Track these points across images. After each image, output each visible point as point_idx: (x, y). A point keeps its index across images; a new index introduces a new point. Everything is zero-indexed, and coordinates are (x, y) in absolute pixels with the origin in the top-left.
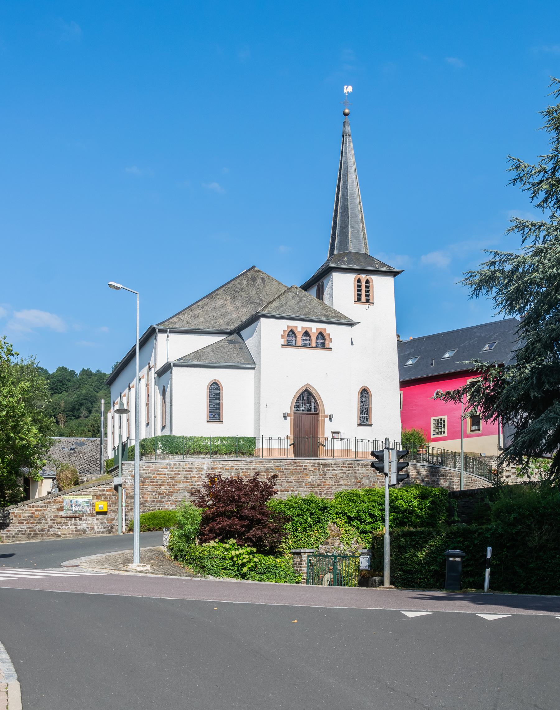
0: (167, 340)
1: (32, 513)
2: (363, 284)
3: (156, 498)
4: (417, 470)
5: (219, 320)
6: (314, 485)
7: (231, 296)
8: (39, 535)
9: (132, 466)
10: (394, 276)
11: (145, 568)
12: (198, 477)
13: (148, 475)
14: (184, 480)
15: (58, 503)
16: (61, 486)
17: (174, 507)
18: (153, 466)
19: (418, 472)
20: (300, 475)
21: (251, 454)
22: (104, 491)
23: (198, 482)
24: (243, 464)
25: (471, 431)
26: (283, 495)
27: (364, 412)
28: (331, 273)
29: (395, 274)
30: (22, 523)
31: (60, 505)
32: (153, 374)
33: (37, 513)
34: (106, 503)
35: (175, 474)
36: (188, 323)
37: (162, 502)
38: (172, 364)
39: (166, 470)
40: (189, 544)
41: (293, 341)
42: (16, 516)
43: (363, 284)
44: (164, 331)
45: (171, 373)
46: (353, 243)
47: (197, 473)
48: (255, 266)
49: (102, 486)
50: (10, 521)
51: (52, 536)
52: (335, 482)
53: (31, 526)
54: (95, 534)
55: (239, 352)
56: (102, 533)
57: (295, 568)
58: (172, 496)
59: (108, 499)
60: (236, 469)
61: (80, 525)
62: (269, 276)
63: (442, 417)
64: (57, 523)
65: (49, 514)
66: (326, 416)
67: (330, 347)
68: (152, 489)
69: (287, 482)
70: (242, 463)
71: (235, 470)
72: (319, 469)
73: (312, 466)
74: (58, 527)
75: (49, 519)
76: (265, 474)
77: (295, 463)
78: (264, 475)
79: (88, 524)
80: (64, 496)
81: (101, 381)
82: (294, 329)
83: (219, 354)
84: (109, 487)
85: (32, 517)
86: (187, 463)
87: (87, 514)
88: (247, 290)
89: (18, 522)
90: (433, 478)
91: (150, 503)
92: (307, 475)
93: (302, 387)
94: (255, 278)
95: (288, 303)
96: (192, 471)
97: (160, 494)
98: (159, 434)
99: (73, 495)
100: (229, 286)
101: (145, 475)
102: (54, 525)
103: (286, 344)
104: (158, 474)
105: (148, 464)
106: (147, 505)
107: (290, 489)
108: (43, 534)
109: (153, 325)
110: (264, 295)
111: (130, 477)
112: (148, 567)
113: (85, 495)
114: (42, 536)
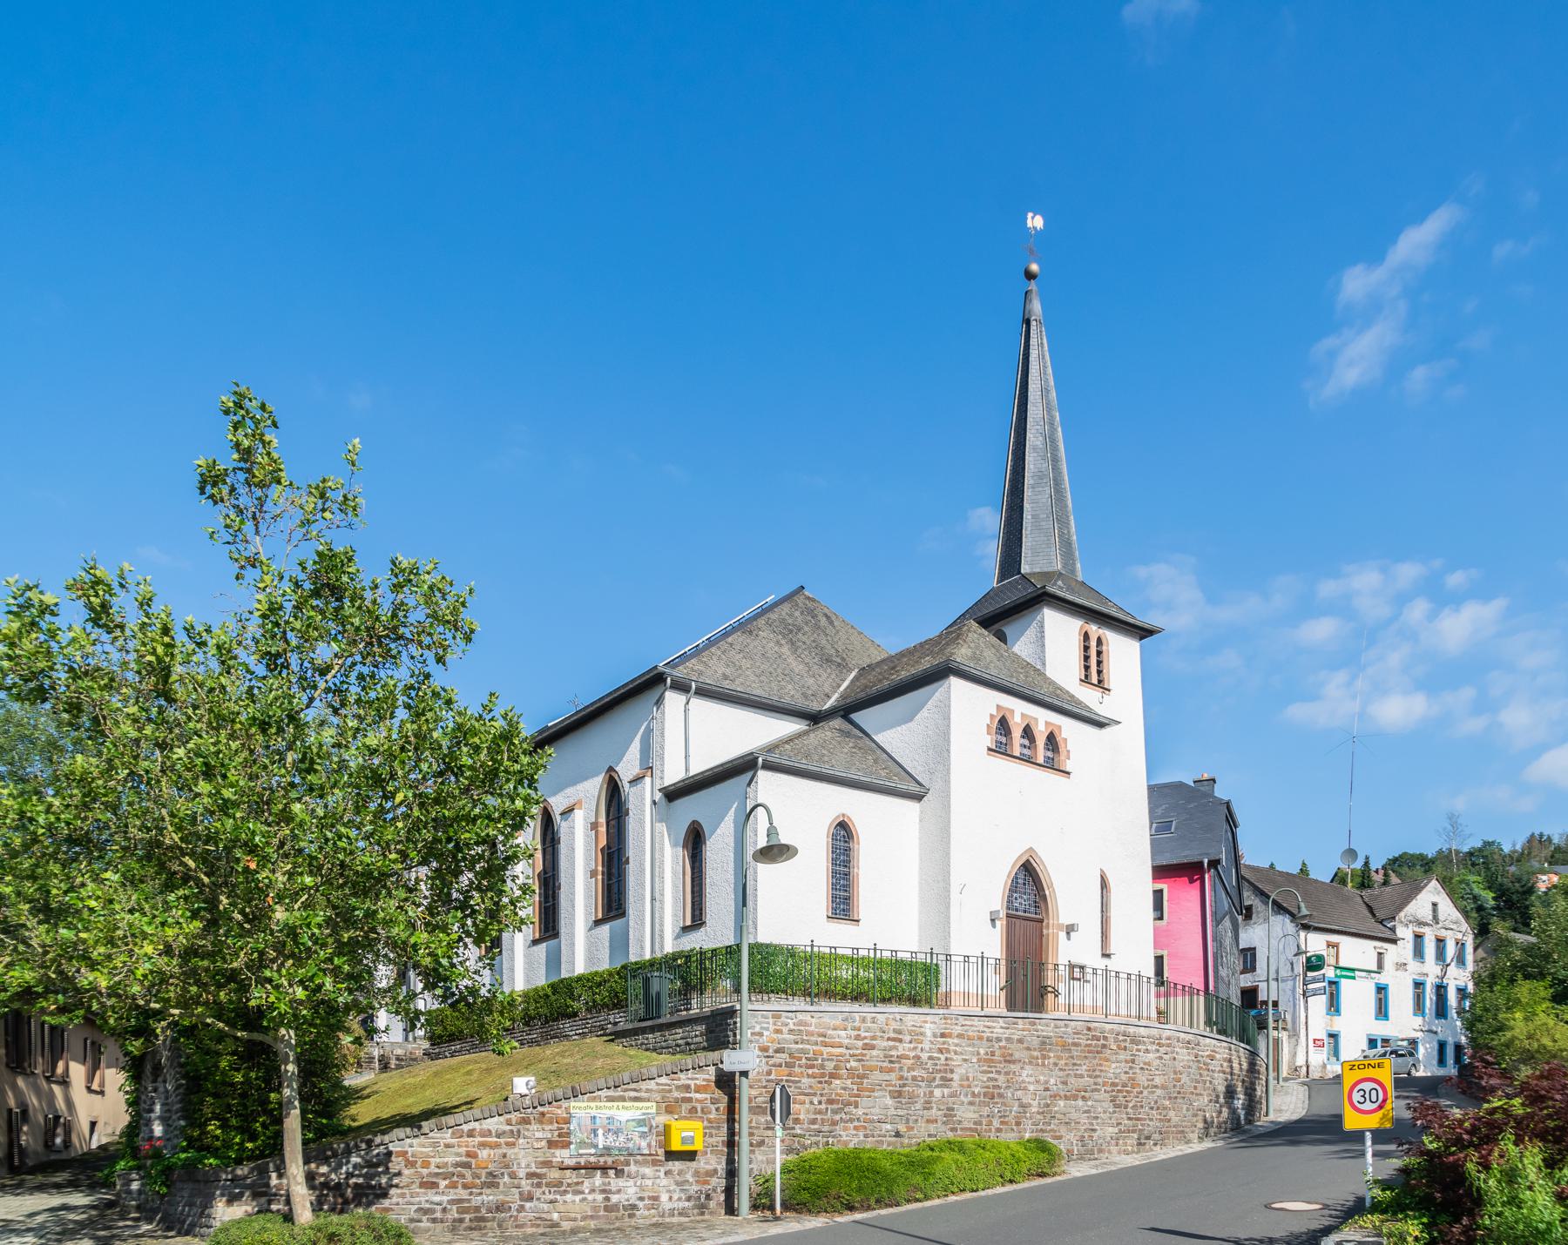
1: (468, 1155)
2: (1093, 644)
3: (820, 1112)
6: (1116, 1085)
8: (489, 1224)
9: (760, 1019)
12: (914, 1057)
13: (801, 1046)
15: (551, 1123)
17: (862, 1138)
18: (813, 1020)
22: (687, 1088)
24: (1002, 1028)
26: (1069, 1110)
28: (1041, 608)
29: (1142, 633)
30: (434, 1185)
31: (559, 1129)
33: (484, 1154)
34: (699, 1125)
36: (725, 677)
37: (834, 1123)
39: (843, 1033)
43: (1093, 644)
44: (681, 687)
47: (912, 1046)
49: (682, 1076)
50: (390, 1179)
51: (532, 1226)
52: (1148, 1080)
53: (462, 1193)
54: (663, 1216)
59: (699, 1114)
60: (989, 1040)
61: (619, 1191)
64: (548, 1185)
65: (524, 1158)
66: (1060, 927)
67: (1068, 770)
69: (1076, 1076)
71: (985, 1042)
72: (1125, 1048)
74: (551, 1197)
75: (522, 1173)
77: (1089, 1029)
79: (642, 1188)
80: (573, 1104)
85: (467, 1165)
86: (891, 1017)
87: (639, 1157)
89: (418, 1181)
96: (900, 1041)
97: (830, 1102)
101: (793, 1046)
102: (538, 1193)
103: (994, 748)
105: (800, 1016)
106: (799, 1132)
108: (504, 1220)
113: (636, 1099)
114: (500, 1226)
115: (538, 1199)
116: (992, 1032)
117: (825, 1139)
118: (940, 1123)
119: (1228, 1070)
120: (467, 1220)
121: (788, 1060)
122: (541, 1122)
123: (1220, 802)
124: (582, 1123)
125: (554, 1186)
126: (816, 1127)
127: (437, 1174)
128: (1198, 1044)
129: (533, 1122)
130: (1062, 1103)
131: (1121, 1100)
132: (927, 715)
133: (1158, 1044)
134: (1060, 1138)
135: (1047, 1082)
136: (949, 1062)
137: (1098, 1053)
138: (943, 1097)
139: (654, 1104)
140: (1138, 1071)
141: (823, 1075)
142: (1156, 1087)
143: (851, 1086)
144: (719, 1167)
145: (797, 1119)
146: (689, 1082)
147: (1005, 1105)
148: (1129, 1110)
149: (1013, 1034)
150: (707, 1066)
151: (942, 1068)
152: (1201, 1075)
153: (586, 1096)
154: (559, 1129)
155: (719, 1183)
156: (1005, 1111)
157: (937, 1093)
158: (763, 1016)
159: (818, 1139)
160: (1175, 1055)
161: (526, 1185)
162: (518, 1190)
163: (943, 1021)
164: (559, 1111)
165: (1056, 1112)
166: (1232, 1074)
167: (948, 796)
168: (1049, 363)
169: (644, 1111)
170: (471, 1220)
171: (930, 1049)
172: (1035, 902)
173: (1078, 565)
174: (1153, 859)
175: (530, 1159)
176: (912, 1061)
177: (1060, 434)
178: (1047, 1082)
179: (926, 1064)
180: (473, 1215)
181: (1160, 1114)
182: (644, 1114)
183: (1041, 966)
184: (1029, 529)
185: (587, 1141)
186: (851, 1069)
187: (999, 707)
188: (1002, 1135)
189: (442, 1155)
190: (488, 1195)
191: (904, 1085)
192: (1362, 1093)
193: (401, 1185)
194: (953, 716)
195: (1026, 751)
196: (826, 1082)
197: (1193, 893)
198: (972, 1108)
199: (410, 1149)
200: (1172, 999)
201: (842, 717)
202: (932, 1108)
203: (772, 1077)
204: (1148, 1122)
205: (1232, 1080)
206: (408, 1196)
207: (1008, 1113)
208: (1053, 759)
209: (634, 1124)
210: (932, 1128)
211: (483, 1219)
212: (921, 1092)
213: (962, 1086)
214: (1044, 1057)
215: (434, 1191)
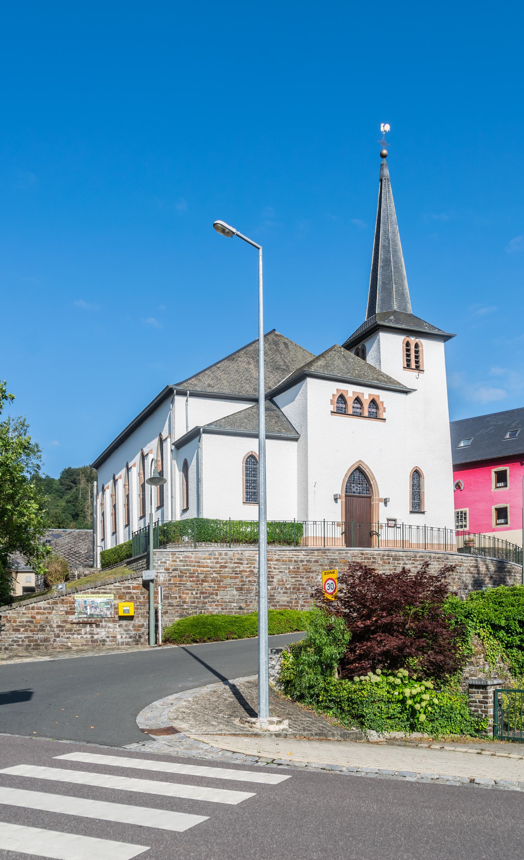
0: (187, 405)
1: (32, 617)
2: (412, 347)
3: (197, 598)
4: (486, 565)
5: (244, 385)
7: (253, 359)
8: (41, 647)
9: (165, 556)
11: (282, 727)
12: (249, 571)
13: (186, 568)
14: (233, 575)
15: (67, 604)
16: (49, 581)
17: (220, 610)
18: (193, 555)
19: (487, 568)
21: (297, 544)
22: (129, 588)
23: (249, 577)
24: (304, 555)
25: (497, 524)
27: (416, 497)
28: (379, 333)
29: (445, 338)
30: (18, 630)
31: (70, 606)
32: (168, 446)
33: (38, 617)
34: (132, 604)
35: (221, 567)
36: (209, 385)
37: (205, 603)
38: (201, 430)
39: (209, 561)
40: (326, 676)
41: (342, 408)
42: (9, 621)
43: (412, 347)
44: (183, 393)
45: (199, 441)
46: (397, 301)
47: (248, 566)
48: (275, 330)
49: (126, 582)
51: (60, 648)
53: (30, 634)
54: (118, 645)
55: (277, 420)
56: (128, 644)
57: (473, 709)
58: (217, 595)
59: (135, 599)
60: (295, 561)
61: (98, 634)
62: (291, 342)
63: (463, 510)
64: (66, 631)
65: (55, 619)
66: (380, 500)
67: (384, 418)
71: (293, 562)
72: (389, 563)
73: (382, 559)
74: (68, 636)
75: (55, 625)
77: (362, 554)
80: (76, 595)
81: (50, 486)
82: (344, 394)
83: (254, 421)
84: (135, 583)
85: (31, 622)
86: (236, 552)
87: (106, 619)
88: (271, 355)
89: (12, 629)
90: (501, 574)
91: (189, 604)
93: (354, 464)
94: (277, 342)
95: (335, 363)
96: (242, 564)
97: (202, 593)
98: (178, 518)
99: (88, 593)
100: (250, 348)
101: (182, 567)
102: (61, 634)
103: (336, 411)
104: (199, 566)
105: (186, 554)
106: (186, 607)
108: (48, 645)
109: (171, 385)
110: (289, 362)
111: (163, 571)
112: (285, 724)
113: (105, 593)
114: (46, 648)
115: (62, 637)
117: (200, 611)
120: (32, 645)
121: (179, 574)
122: (62, 603)
124: (80, 604)
125: (68, 631)
126: (195, 605)
127: (19, 626)
129: (59, 603)
139: (113, 595)
141: (198, 581)
143: (213, 586)
144: (145, 624)
146: (130, 585)
150: (138, 578)
153: (82, 592)
154: (70, 606)
155: (145, 631)
158: (166, 554)
161: (57, 631)
162: (53, 633)
164: (70, 599)
169: (108, 598)
170: (34, 645)
174: (453, 462)
175: (58, 619)
176: (248, 573)
180: (35, 643)
182: (108, 600)
183: (369, 522)
184: (380, 289)
185: (82, 611)
187: (338, 390)
189: (21, 617)
190: (41, 635)
191: (244, 585)
192: (328, 585)
193: (5, 630)
194: (308, 398)
196: (200, 584)
198: (286, 595)
199: (8, 615)
203: (172, 582)
206: (8, 635)
209: (104, 604)
211: (38, 645)
212: (254, 587)
213: (279, 584)
215: (18, 633)
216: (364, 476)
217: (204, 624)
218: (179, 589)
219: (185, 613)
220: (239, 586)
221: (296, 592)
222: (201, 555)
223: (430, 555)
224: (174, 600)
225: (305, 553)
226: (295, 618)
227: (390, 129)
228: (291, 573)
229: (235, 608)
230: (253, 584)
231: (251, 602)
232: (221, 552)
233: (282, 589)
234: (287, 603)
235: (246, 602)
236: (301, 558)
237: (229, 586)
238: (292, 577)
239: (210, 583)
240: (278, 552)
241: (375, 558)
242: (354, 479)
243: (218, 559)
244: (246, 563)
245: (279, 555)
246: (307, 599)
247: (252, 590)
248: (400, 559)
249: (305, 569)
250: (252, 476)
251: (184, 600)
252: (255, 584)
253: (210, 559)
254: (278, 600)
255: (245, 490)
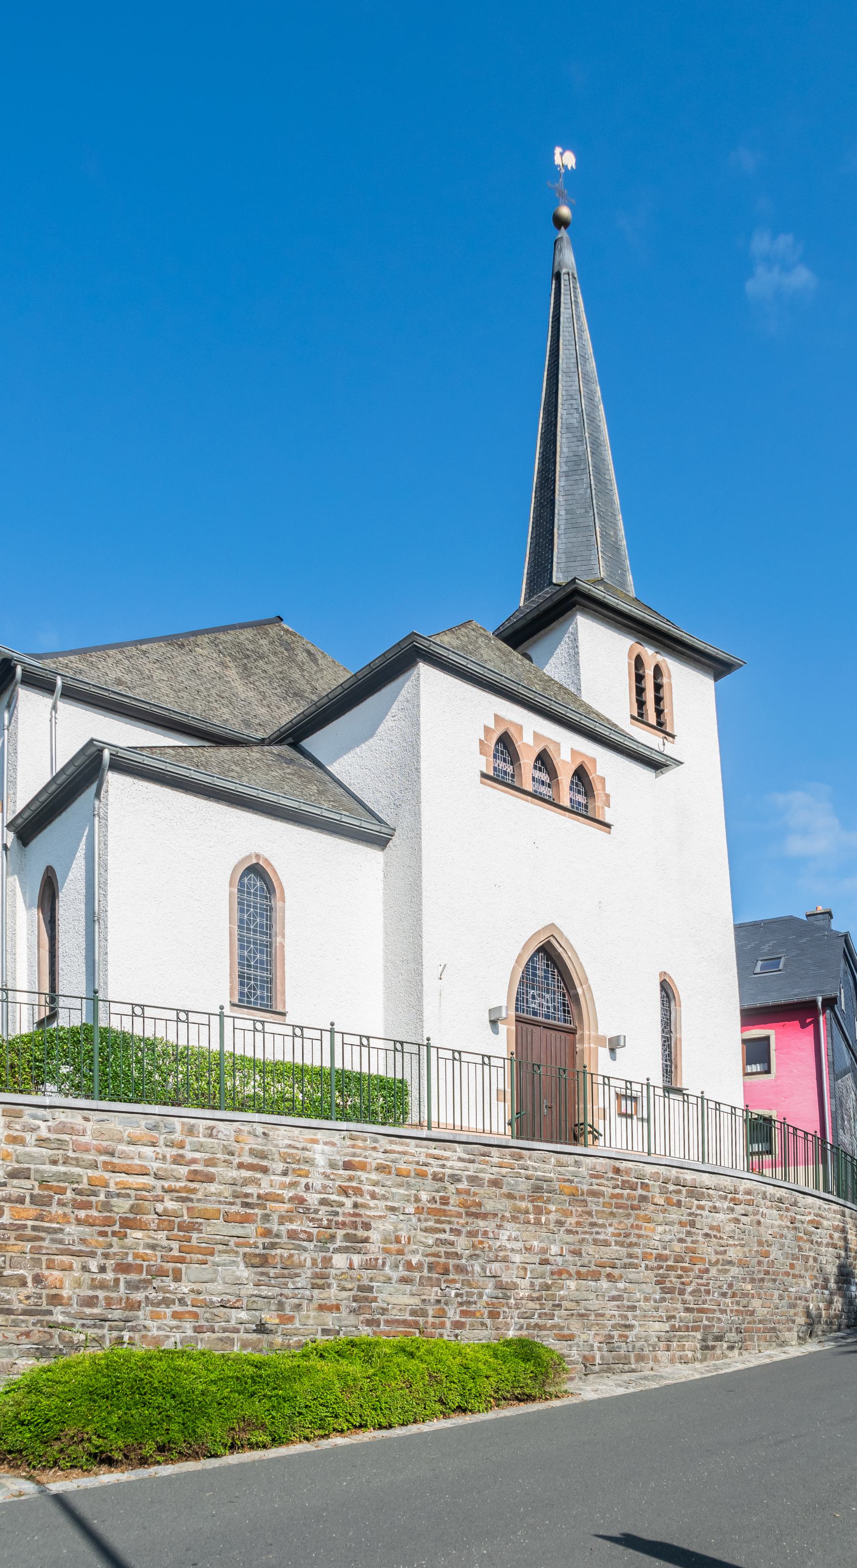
2: (649, 673)
3: (103, 1286)
5: (215, 705)
10: (717, 677)
12: (291, 1199)
13: (62, 1169)
17: (190, 1333)
18: (89, 1126)
20: (631, 1220)
23: (291, 1221)
24: (461, 1159)
26: (585, 1295)
35: (194, 1177)
36: (119, 682)
38: (106, 754)
39: (148, 1151)
43: (649, 673)
45: (98, 795)
47: (287, 1180)
52: (717, 1253)
60: (436, 1178)
66: (600, 1041)
68: (83, 1241)
69: (596, 1242)
70: (455, 1156)
71: (429, 1181)
72: (679, 1204)
76: (530, 1206)
77: (617, 1171)
78: (527, 1212)
82: (513, 733)
86: (246, 1128)
91: (75, 1308)
92: (649, 1220)
96: (265, 1170)
97: (125, 1268)
101: (48, 1167)
105: (62, 1116)
106: (61, 1318)
107: (603, 1270)
116: (443, 1166)
117: (115, 1334)
118: (344, 1312)
119: (841, 1243)
121: (36, 1191)
123: (837, 935)
126: (96, 1311)
128: (795, 1204)
130: (572, 1284)
131: (673, 1280)
132: (391, 724)
133: (733, 1199)
134: (570, 1338)
135: (544, 1251)
136: (362, 1211)
137: (633, 1208)
138: (351, 1267)
140: (700, 1238)
141: (108, 1222)
142: (730, 1263)
143: (165, 1243)
145: (55, 1296)
147: (470, 1285)
148: (687, 1297)
149: (482, 1171)
151: (348, 1220)
152: (800, 1249)
156: (470, 1294)
157: (340, 1261)
159: (100, 1332)
160: (759, 1217)
163: (349, 1142)
165: (562, 1298)
166: (846, 1249)
167: (419, 836)
168: (586, 326)
171: (325, 1187)
172: (564, 1005)
173: (630, 578)
176: (287, 1206)
177: (602, 412)
178: (544, 1251)
179: (316, 1211)
181: (738, 1303)
184: (562, 527)
186: (166, 1213)
187: (498, 719)
188: (465, 1333)
191: (273, 1246)
195: (544, 790)
196: (114, 1234)
197: (806, 1039)
200: (792, 1169)
201: (290, 745)
202: (329, 1286)
204: (718, 1315)
205: (847, 1257)
207: (475, 1298)
208: (586, 807)
210: (330, 1320)
213: (386, 1251)
214: (538, 1211)
216: (559, 972)
217: (138, 1387)
218: (36, 1250)
219: (56, 1341)
220: (257, 1251)
221: (439, 1280)
222: (120, 1128)
223: (763, 1189)
224: (14, 1291)
225: (465, 1152)
226: (455, 1369)
227: (576, 164)
228: (422, 1217)
229: (242, 1327)
230: (305, 1244)
231: (298, 1307)
232: (192, 1121)
233: (397, 1266)
234: (411, 1314)
235: (281, 1306)
236: (451, 1168)
237: (220, 1247)
238: (426, 1230)
239: (152, 1233)
240: (383, 1140)
241: (647, 1185)
242: (534, 975)
243: (182, 1147)
244: (279, 1171)
245: (385, 1152)
246: (469, 1303)
247: (302, 1265)
248: (703, 1193)
249: (463, 1205)
250: (255, 931)
251: (54, 1292)
252: (311, 1246)
253: (154, 1145)
254: (385, 1305)
255: (237, 968)
